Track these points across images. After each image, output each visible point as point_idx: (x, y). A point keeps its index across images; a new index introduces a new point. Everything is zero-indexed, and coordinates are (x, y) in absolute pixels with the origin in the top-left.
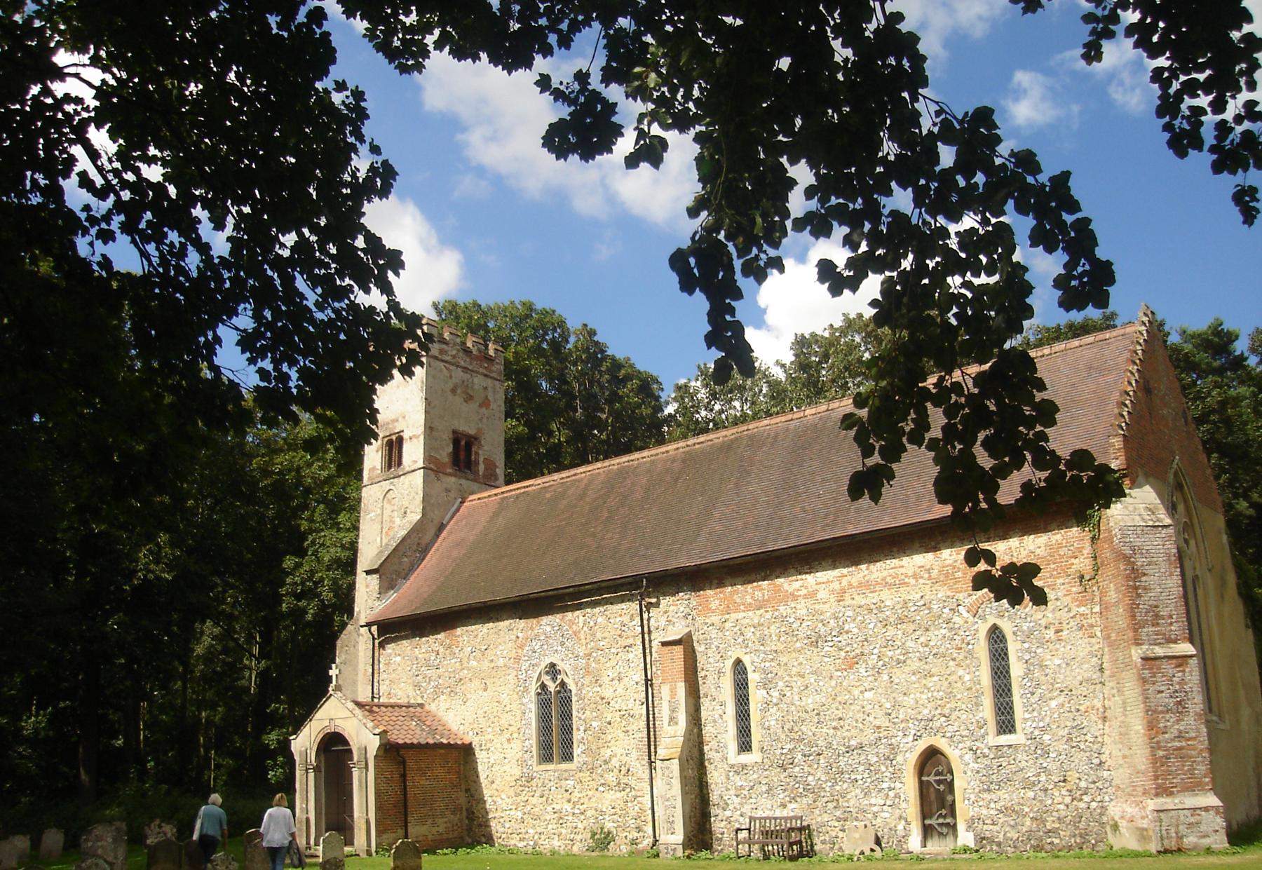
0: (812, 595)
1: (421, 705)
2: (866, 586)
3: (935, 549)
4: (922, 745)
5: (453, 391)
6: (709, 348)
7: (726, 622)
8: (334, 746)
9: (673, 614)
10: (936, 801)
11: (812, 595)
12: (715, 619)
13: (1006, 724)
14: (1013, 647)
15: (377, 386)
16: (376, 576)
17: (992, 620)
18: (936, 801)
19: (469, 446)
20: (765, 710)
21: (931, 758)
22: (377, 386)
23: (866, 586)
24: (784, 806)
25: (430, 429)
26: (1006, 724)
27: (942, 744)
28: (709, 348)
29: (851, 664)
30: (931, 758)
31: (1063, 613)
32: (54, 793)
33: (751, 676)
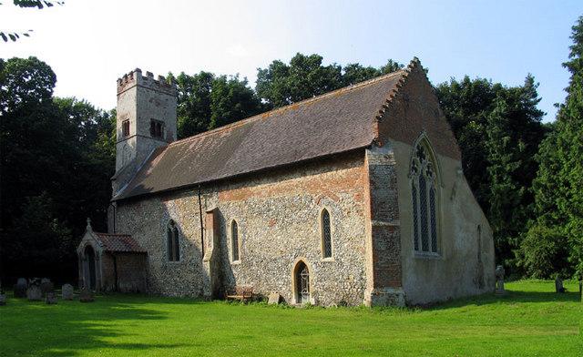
0: (259, 193)
1: (130, 236)
2: (279, 190)
3: (305, 175)
4: (298, 260)
5: (151, 101)
6: (416, 64)
7: (228, 203)
8: (89, 249)
9: (213, 202)
10: (301, 284)
11: (259, 193)
12: (225, 203)
13: (328, 253)
14: (331, 219)
15: (252, 85)
16: (211, 215)
17: (324, 207)
18: (301, 284)
19: (159, 125)
20: (243, 242)
21: (301, 267)
22: (252, 85)
23: (279, 190)
24: (249, 283)
25: (139, 118)
26: (328, 253)
27: (305, 260)
28: (416, 64)
29: (272, 225)
30: (301, 267)
31: (351, 205)
32: (30, 311)
33: (239, 228)
